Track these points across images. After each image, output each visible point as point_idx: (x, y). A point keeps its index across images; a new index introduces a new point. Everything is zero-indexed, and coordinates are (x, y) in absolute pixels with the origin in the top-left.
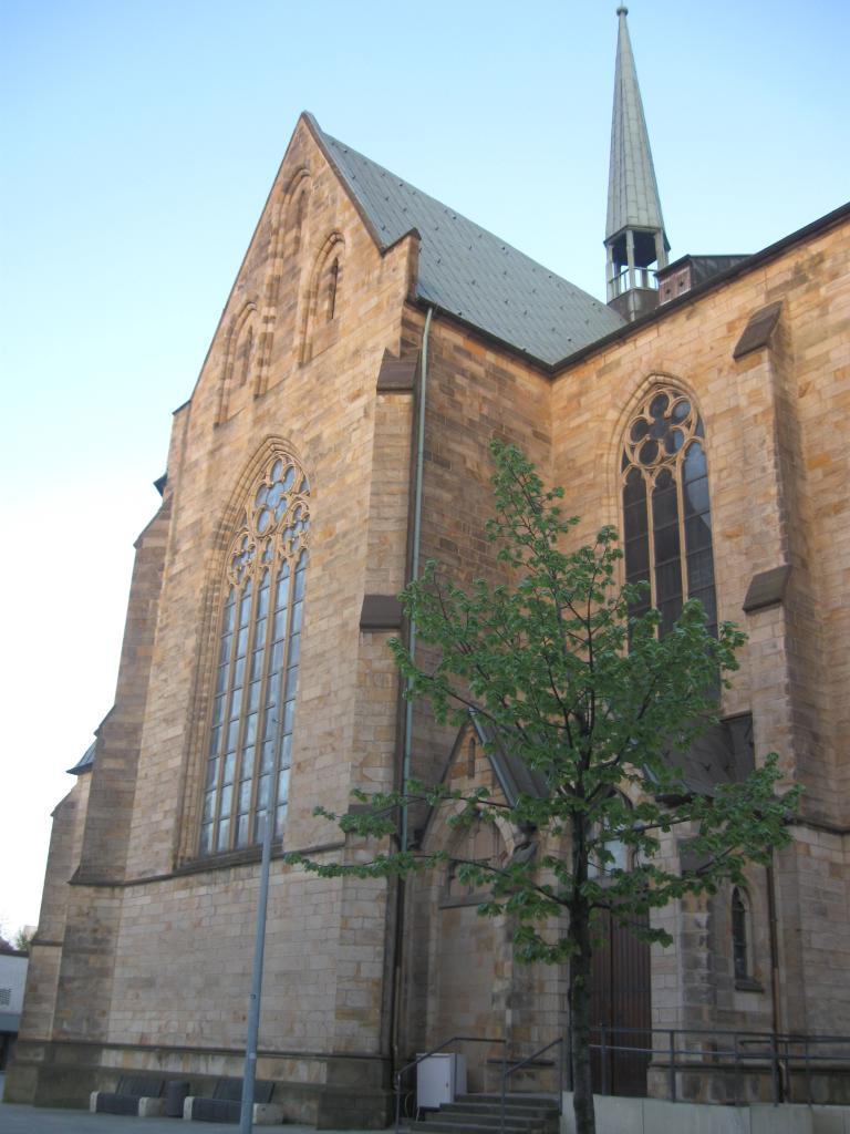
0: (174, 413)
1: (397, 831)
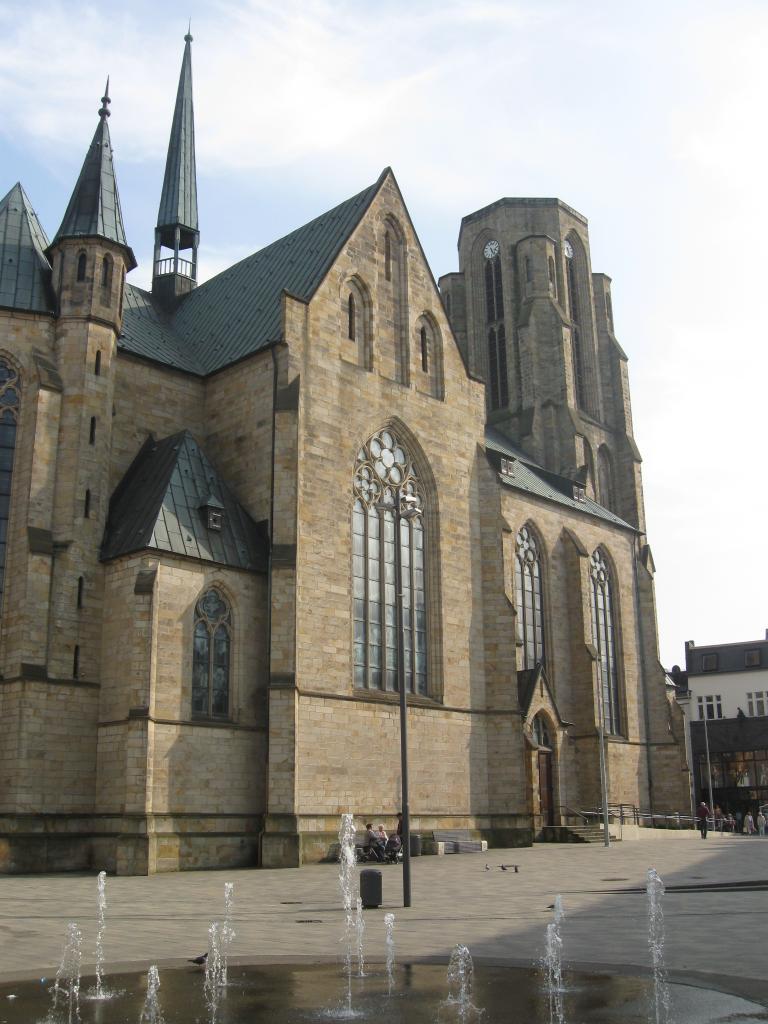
0: (467, 221)
1: (52, 675)
